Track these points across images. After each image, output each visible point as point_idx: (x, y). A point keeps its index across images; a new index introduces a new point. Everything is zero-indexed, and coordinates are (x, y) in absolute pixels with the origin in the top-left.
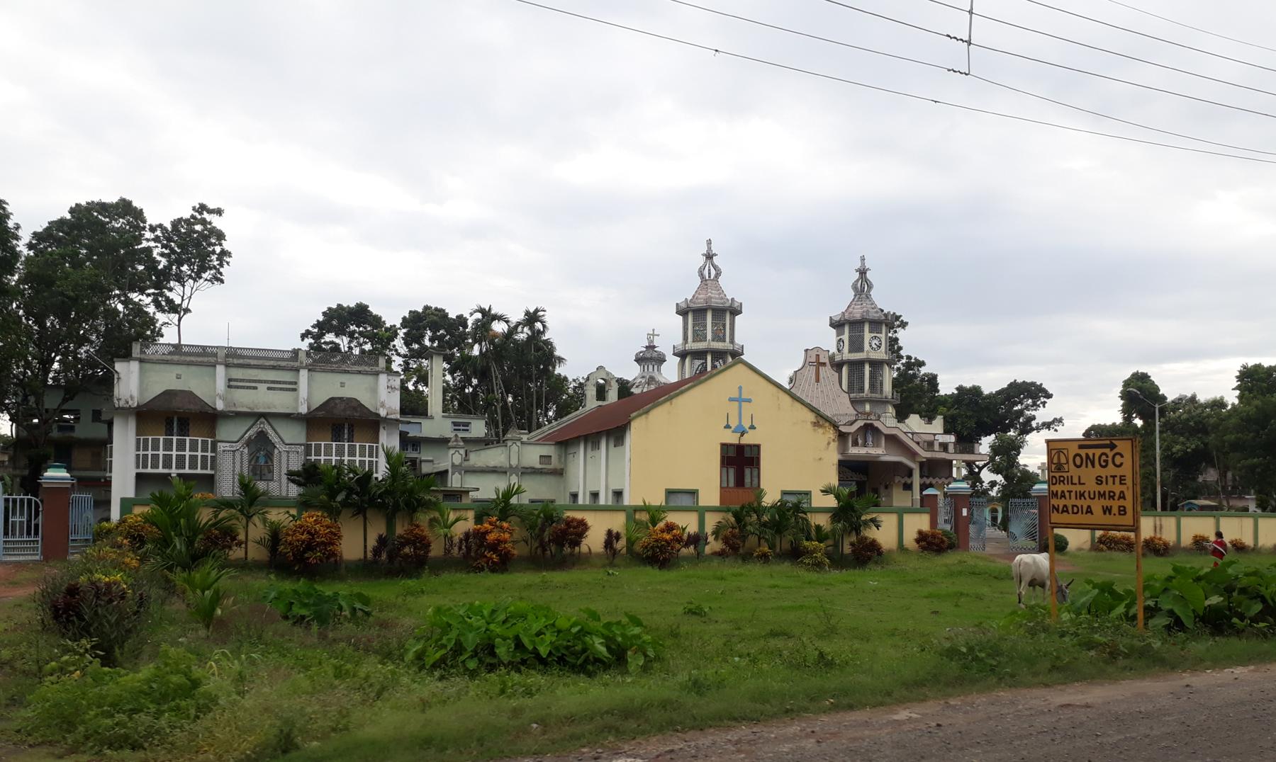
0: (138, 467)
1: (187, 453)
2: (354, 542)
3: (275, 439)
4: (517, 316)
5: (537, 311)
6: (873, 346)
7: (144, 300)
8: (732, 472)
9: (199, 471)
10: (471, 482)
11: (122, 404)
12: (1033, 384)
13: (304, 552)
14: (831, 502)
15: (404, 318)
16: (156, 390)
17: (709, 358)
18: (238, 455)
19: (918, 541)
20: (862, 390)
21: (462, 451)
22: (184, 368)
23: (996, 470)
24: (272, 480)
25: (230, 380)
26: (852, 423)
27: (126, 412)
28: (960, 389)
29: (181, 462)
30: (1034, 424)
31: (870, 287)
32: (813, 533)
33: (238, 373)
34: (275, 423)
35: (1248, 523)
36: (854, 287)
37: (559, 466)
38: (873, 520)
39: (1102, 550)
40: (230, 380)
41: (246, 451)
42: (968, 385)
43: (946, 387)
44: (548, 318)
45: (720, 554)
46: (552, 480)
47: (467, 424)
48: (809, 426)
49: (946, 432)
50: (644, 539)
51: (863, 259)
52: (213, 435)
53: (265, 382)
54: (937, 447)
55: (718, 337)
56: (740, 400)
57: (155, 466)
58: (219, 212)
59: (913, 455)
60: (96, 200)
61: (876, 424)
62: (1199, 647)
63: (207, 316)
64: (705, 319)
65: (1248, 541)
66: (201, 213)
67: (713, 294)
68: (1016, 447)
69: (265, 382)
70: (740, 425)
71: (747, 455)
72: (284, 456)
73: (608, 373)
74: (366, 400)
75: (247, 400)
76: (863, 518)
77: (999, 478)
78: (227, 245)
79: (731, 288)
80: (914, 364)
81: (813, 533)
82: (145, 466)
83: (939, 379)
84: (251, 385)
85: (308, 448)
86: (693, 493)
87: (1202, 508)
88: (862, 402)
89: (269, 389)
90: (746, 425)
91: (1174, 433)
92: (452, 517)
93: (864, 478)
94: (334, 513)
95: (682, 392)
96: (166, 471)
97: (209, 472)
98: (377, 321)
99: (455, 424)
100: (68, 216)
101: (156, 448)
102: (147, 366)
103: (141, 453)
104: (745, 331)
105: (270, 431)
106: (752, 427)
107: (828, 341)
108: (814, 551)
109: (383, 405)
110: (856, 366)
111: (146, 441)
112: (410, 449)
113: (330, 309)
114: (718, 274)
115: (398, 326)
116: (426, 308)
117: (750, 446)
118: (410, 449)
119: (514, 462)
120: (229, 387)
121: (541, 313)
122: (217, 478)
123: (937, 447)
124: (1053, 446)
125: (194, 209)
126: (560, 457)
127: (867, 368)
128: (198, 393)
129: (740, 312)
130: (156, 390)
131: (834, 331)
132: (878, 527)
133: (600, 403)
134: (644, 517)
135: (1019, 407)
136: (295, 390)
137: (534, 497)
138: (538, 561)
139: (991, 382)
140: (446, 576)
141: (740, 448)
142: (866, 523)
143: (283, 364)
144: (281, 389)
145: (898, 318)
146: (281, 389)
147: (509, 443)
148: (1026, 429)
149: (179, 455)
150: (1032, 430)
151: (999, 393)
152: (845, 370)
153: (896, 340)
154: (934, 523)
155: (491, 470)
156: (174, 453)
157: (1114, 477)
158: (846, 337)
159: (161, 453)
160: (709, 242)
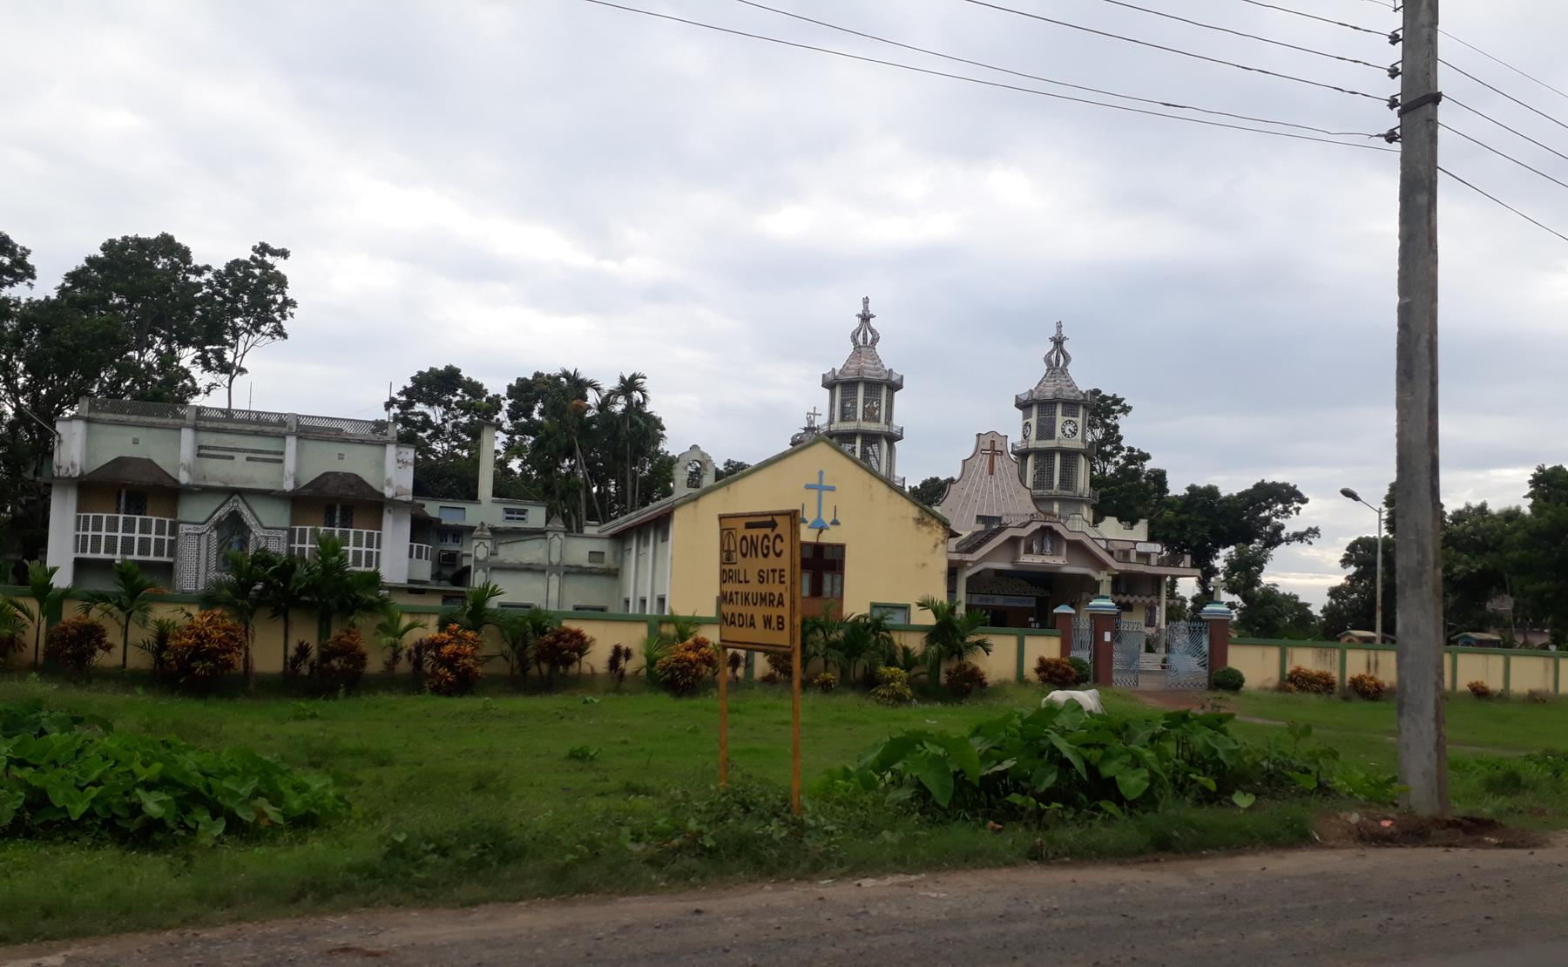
1: (137, 535)
2: (268, 651)
4: (610, 383)
5: (634, 377)
6: (1071, 432)
7: (187, 356)
9: (152, 558)
10: (501, 581)
11: (62, 473)
12: (1285, 486)
13: (192, 659)
14: (928, 618)
15: (510, 387)
16: (311, 474)
17: (858, 441)
18: (204, 539)
19: (1038, 671)
20: (1051, 486)
23: (1232, 591)
25: (200, 447)
26: (1024, 525)
27: (67, 482)
28: (1192, 489)
29: (128, 545)
31: (1067, 359)
32: (900, 657)
33: (209, 439)
35: (1496, 662)
36: (1048, 360)
38: (981, 643)
39: (1290, 690)
40: (200, 447)
41: (215, 534)
43: (1177, 487)
45: (768, 680)
46: (604, 582)
47: (523, 512)
48: (911, 523)
49: (1152, 538)
50: (665, 658)
51: (1059, 326)
52: (174, 515)
53: (245, 451)
54: (1133, 557)
55: (870, 415)
56: (820, 488)
57: (96, 549)
58: (284, 254)
59: (1103, 566)
60: (131, 235)
61: (1056, 527)
62: (960, 834)
63: (266, 377)
65: (1494, 684)
67: (867, 364)
68: (1258, 562)
69: (245, 451)
70: (819, 519)
71: (828, 555)
73: (703, 454)
74: (369, 476)
75: (219, 472)
76: (968, 640)
77: (1236, 599)
78: (289, 294)
79: (890, 356)
80: (1136, 458)
81: (900, 657)
82: (84, 550)
83: (1168, 477)
84: (227, 454)
85: (291, 533)
87: (1481, 643)
88: (1050, 500)
91: (1458, 550)
92: (406, 621)
93: (1047, 594)
94: (245, 615)
96: (109, 556)
97: (165, 559)
98: (475, 389)
99: (508, 511)
100: (101, 255)
101: (97, 527)
102: (96, 427)
104: (905, 410)
105: (246, 513)
106: (835, 523)
107: (1013, 429)
108: (892, 679)
109: (389, 483)
110: (1044, 456)
112: (450, 540)
113: (420, 373)
114: (875, 340)
115: (504, 395)
118: (450, 540)
119: (555, 559)
120: (199, 455)
122: (177, 567)
123: (1133, 557)
124: (729, 524)
125: (254, 249)
126: (615, 554)
127: (1058, 458)
128: (158, 461)
131: (1020, 412)
132: (987, 651)
134: (669, 630)
135: (1267, 513)
137: (579, 603)
138: (520, 683)
139: (1231, 484)
140: (384, 698)
142: (970, 647)
143: (268, 429)
145: (1117, 401)
147: (550, 535)
148: (1274, 539)
149: (129, 537)
150: (1281, 541)
151: (1241, 495)
152: (1030, 460)
153: (1116, 427)
154: (1066, 648)
155: (532, 571)
156: (120, 534)
157: (774, 571)
158: (1033, 421)
159: (104, 533)
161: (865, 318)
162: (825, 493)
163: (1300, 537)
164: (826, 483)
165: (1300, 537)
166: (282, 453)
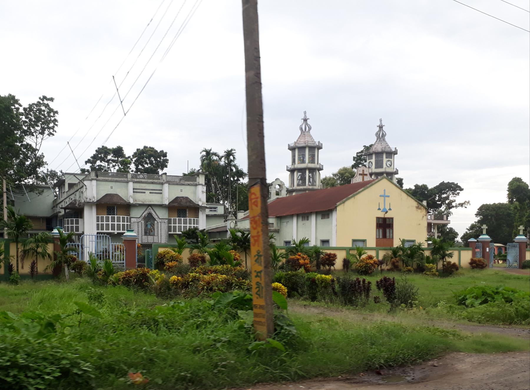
0: (98, 229)
3: (156, 217)
4: (222, 153)
5: (232, 150)
8: (381, 231)
12: (453, 183)
18: (140, 224)
19: (471, 264)
21: (234, 222)
22: (114, 183)
24: (154, 235)
25: (134, 189)
27: (90, 204)
30: (454, 204)
33: (138, 186)
34: (155, 209)
37: (277, 228)
42: (420, 184)
44: (236, 155)
47: (216, 208)
48: (415, 208)
51: (381, 121)
55: (312, 161)
56: (384, 196)
57: (108, 229)
58: (52, 99)
64: (305, 152)
66: (43, 100)
71: (388, 222)
72: (159, 224)
73: (281, 182)
74: (191, 197)
79: (316, 137)
82: (109, 230)
83: (403, 181)
85: (169, 222)
86: (364, 241)
89: (150, 193)
90: (387, 208)
95: (359, 193)
96: (113, 231)
102: (99, 182)
103: (129, 223)
104: (323, 157)
106: (390, 209)
110: (302, 171)
111: (102, 218)
113: (99, 148)
114: (310, 128)
116: (145, 147)
117: (389, 218)
121: (233, 152)
126: (277, 224)
127: (307, 172)
128: (120, 195)
129: (322, 148)
130: (103, 194)
133: (278, 197)
136: (161, 193)
141: (384, 219)
144: (156, 193)
146: (156, 193)
149: (115, 222)
150: (453, 207)
151: (435, 188)
156: (74, 225)
160: (305, 113)
161: (381, 127)
162: (386, 198)
163: (461, 205)
164: (387, 194)
165: (461, 205)
166: (161, 190)
